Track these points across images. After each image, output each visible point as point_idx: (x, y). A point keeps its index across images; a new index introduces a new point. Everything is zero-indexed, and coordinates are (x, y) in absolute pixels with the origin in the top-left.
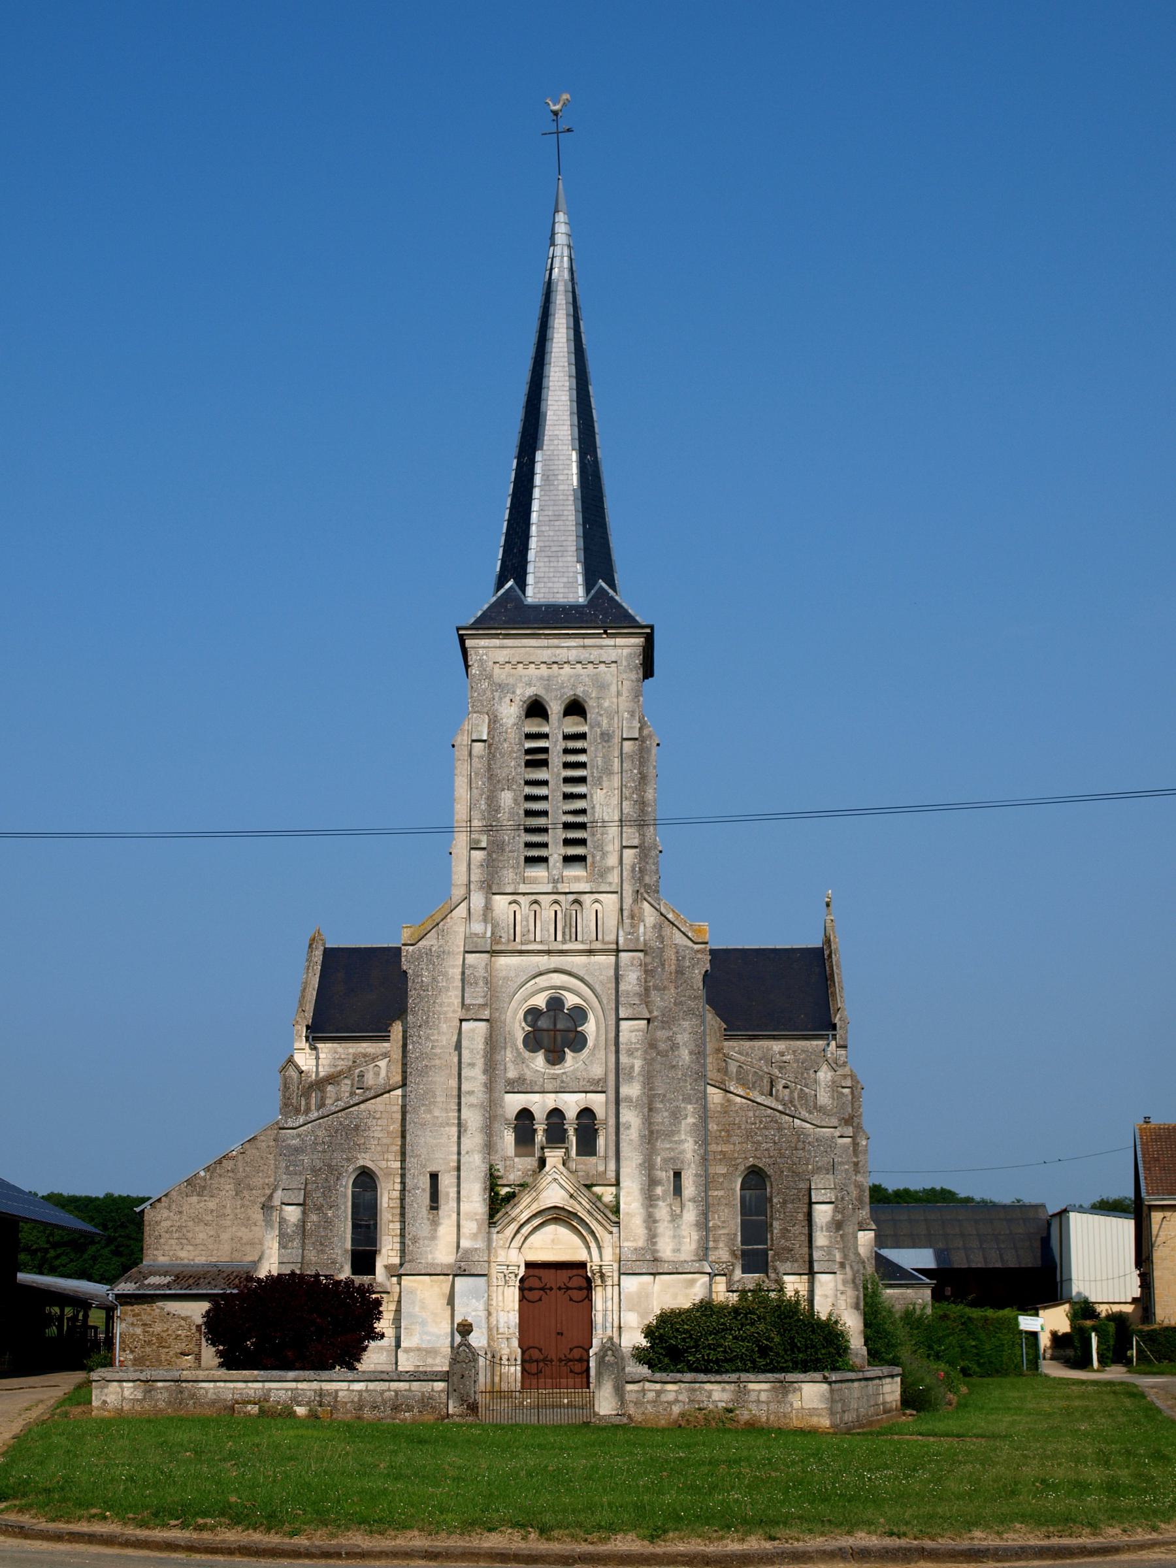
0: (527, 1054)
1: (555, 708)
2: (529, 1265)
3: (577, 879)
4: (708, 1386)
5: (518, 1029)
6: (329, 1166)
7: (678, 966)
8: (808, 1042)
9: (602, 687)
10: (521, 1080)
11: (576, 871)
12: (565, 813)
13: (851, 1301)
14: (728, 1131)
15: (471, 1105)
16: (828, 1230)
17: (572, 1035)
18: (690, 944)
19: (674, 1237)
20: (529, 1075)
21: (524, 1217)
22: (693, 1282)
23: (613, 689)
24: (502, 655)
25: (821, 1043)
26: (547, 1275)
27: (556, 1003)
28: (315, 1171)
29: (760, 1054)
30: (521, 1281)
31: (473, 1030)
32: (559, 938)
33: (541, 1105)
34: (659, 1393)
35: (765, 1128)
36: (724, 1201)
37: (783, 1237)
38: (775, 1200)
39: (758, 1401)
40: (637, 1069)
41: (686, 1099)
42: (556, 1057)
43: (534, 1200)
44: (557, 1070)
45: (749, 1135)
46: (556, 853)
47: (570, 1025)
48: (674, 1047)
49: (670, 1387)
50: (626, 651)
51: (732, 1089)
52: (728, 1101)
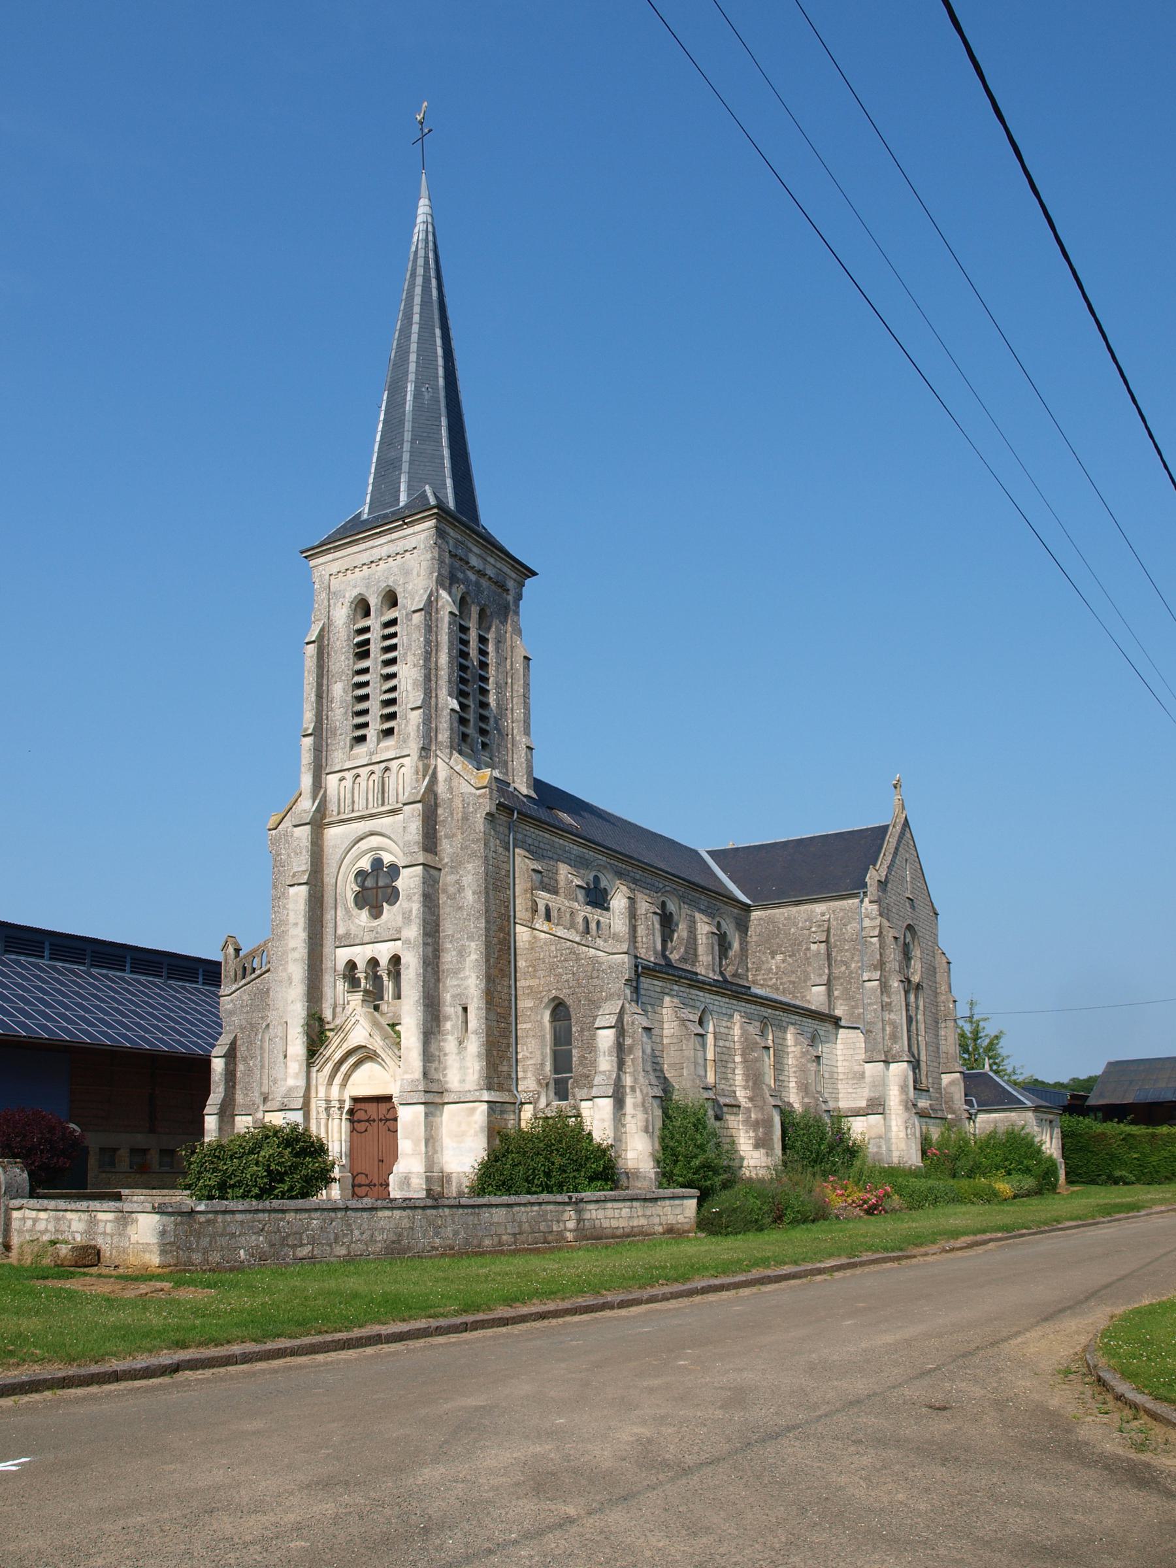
0: (355, 911)
1: (373, 602)
2: (355, 1100)
3: (387, 749)
4: (69, 1215)
5: (349, 889)
6: (251, 1024)
7: (464, 813)
8: (845, 902)
9: (407, 572)
10: (348, 935)
11: (390, 742)
12: (385, 692)
13: (641, 1124)
14: (534, 966)
15: (296, 960)
16: (610, 1055)
17: (389, 890)
18: (474, 791)
19: (460, 1068)
21: (337, 1056)
22: (473, 1110)
23: (415, 573)
24: (334, 568)
25: (856, 901)
26: (371, 1107)
27: (377, 863)
28: (242, 1029)
29: (805, 916)
30: (351, 1112)
31: (297, 894)
32: (370, 805)
33: (360, 955)
34: (35, 1220)
35: (566, 960)
36: (531, 1033)
37: (581, 1064)
38: (574, 1029)
39: (104, 1233)
40: (414, 912)
41: (471, 938)
42: (376, 913)
43: (343, 1040)
44: (376, 923)
45: (552, 968)
46: (371, 733)
47: (388, 881)
48: (461, 889)
49: (43, 1215)
50: (423, 535)
51: (537, 926)
52: (535, 937)
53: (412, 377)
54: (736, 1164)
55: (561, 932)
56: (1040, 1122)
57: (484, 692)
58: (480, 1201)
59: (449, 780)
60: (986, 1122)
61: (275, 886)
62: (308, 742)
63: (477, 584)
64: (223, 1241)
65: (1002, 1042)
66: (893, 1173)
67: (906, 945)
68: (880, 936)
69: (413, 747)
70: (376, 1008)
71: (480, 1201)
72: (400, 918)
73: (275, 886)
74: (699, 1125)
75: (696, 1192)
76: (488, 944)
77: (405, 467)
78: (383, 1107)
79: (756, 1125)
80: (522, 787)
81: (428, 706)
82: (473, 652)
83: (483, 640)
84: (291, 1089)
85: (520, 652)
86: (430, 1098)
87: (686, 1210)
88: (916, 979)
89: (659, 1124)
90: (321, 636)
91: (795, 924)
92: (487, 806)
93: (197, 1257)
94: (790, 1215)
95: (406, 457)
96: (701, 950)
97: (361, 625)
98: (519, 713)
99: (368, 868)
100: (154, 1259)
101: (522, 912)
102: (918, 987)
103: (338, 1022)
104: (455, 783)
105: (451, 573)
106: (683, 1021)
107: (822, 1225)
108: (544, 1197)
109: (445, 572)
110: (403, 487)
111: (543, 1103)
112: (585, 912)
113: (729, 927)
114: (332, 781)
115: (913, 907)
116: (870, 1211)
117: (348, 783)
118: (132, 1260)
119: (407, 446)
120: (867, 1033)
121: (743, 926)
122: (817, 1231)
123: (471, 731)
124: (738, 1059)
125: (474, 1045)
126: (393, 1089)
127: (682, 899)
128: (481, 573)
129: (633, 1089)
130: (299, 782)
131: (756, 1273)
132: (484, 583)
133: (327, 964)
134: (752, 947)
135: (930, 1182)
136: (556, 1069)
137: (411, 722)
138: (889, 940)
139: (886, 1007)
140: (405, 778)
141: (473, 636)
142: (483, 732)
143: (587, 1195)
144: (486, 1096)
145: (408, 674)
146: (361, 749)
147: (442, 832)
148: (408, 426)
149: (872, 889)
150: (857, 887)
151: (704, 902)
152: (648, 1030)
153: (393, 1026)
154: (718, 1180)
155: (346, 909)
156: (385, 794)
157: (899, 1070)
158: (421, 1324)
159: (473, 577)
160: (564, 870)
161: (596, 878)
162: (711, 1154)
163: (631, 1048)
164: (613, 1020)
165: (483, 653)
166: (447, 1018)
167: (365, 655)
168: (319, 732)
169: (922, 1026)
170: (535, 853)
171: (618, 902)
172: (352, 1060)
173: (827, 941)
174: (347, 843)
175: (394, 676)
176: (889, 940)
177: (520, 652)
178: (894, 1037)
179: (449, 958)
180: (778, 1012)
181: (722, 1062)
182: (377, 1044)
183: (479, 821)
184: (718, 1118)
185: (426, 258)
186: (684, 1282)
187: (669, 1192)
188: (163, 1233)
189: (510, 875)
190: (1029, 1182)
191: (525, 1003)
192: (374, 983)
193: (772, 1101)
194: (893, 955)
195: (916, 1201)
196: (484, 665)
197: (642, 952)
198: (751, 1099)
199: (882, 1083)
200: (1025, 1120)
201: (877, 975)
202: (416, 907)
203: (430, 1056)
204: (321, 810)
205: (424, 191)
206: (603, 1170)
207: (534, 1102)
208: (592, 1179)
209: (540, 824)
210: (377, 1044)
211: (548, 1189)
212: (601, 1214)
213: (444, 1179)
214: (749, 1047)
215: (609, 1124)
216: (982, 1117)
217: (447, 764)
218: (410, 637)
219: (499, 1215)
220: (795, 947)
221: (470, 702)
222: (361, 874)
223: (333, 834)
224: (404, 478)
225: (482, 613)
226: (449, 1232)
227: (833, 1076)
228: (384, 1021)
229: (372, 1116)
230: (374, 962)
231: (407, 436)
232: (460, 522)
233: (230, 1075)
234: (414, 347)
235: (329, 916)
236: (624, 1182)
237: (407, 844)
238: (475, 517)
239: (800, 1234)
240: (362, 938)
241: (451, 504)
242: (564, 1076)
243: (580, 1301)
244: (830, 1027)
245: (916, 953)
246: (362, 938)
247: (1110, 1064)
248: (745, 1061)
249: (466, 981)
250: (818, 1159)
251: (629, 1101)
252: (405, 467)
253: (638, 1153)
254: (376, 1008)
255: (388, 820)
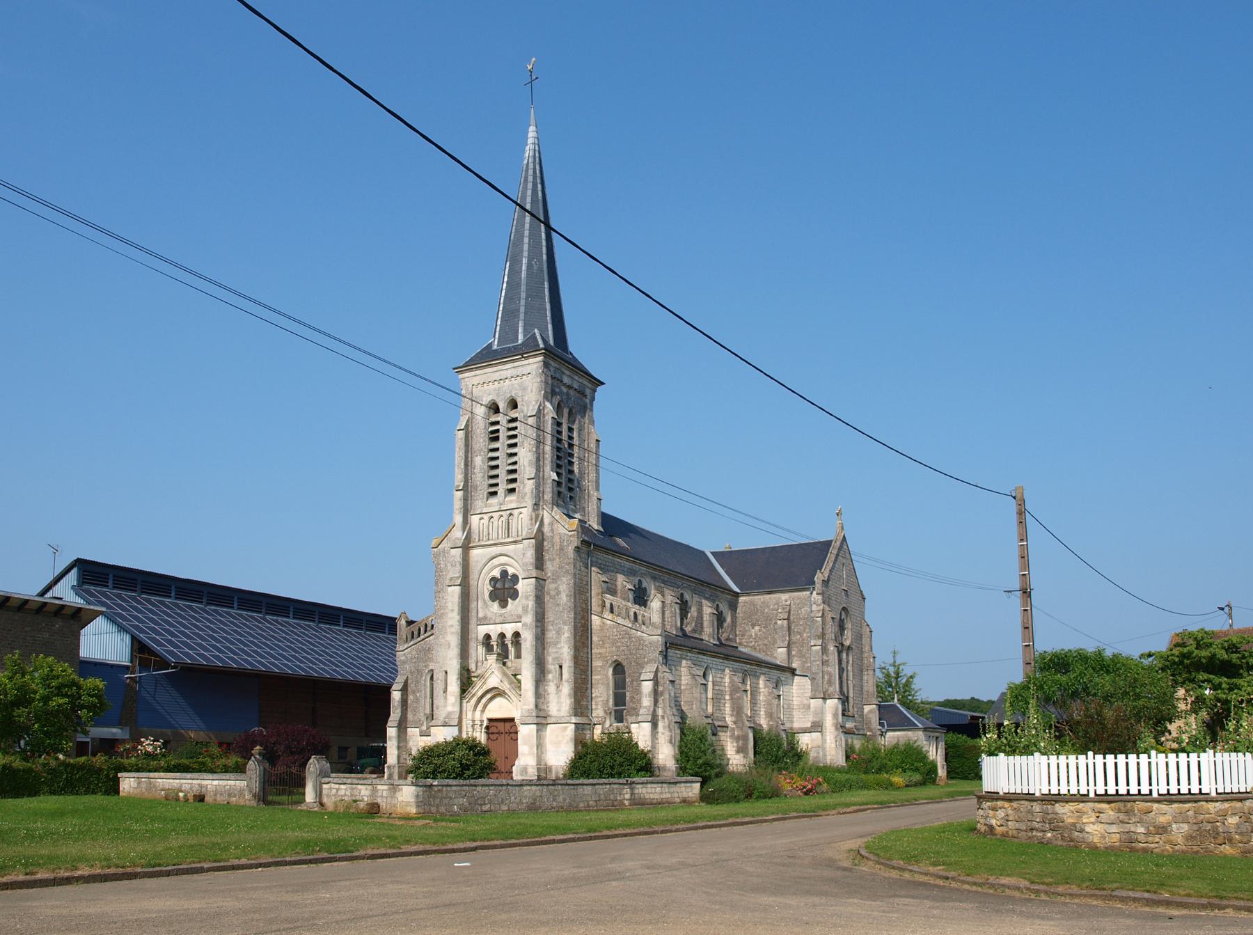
0: (490, 603)
1: (502, 406)
2: (490, 720)
3: (511, 502)
5: (486, 589)
9: (524, 389)
10: (485, 618)
11: (512, 497)
20: (489, 615)
21: (480, 694)
22: (565, 728)
24: (475, 381)
26: (500, 726)
28: (412, 673)
30: (487, 728)
33: (494, 630)
34: (338, 790)
41: (565, 623)
42: (504, 604)
43: (484, 683)
44: (503, 611)
46: (501, 490)
48: (559, 593)
53: (525, 254)
54: (725, 762)
55: (620, 620)
56: (928, 738)
57: (571, 463)
58: (569, 782)
59: (551, 524)
60: (893, 737)
61: (436, 584)
62: (460, 493)
63: (567, 394)
64: (446, 801)
65: (915, 680)
66: (825, 771)
67: (841, 621)
68: (823, 616)
69: (529, 502)
70: (504, 664)
71: (569, 782)
72: (520, 609)
73: (436, 584)
74: (703, 739)
75: (700, 779)
76: (575, 628)
77: (522, 316)
78: (508, 725)
79: (738, 739)
80: (595, 524)
81: (539, 478)
82: (565, 436)
83: (570, 430)
84: (450, 713)
85: (594, 437)
86: (540, 720)
87: (693, 789)
88: (847, 643)
89: (678, 738)
90: (467, 426)
91: (768, 607)
92: (576, 542)
93: (433, 809)
94: (756, 794)
95: (522, 309)
96: (706, 624)
97: (493, 419)
98: (593, 476)
99: (498, 576)
100: (413, 810)
101: (595, 603)
102: (849, 648)
103: (479, 672)
104: (555, 526)
105: (553, 389)
106: (694, 676)
107: (776, 800)
108: (612, 780)
109: (549, 390)
110: (520, 330)
111: (607, 724)
112: (635, 608)
113: (724, 608)
114: (474, 520)
115: (847, 595)
116: (806, 793)
117: (485, 521)
118: (399, 810)
119: (523, 302)
120: (812, 679)
121: (733, 607)
122: (772, 804)
123: (563, 489)
124: (727, 697)
125: (566, 689)
126: (516, 715)
127: (694, 591)
128: (570, 387)
129: (663, 717)
130: (452, 518)
131: (730, 820)
132: (572, 392)
133: (472, 635)
134: (739, 621)
135: (848, 776)
136: (616, 704)
137: (527, 487)
138: (829, 619)
139: (824, 663)
140: (523, 520)
141: (565, 428)
142: (570, 489)
143: (636, 779)
144: (574, 720)
145: (525, 455)
146: (493, 500)
147: (546, 557)
148: (523, 288)
149: (818, 586)
150: (809, 584)
151: (708, 592)
152: (672, 682)
153: (515, 675)
154: (713, 772)
155: (485, 602)
156: (511, 529)
157: (833, 704)
158: (571, 836)
159: (565, 390)
160: (620, 578)
161: (640, 582)
162: (709, 757)
163: (662, 693)
164: (651, 676)
165: (571, 438)
166: (550, 672)
167: (496, 439)
168: (467, 489)
169: (851, 674)
170: (604, 569)
171: (655, 604)
172: (488, 696)
173: (788, 619)
174: (484, 561)
175: (515, 454)
176: (829, 619)
177: (594, 437)
178: (830, 683)
179: (551, 635)
180: (753, 665)
181: (718, 699)
182: (505, 686)
183: (570, 551)
184: (714, 734)
185: (534, 169)
186: (693, 824)
187: (684, 779)
188: (417, 796)
189: (589, 583)
190: (917, 777)
191: (597, 663)
192: (504, 648)
193: (748, 724)
194: (831, 629)
195: (838, 787)
196: (571, 446)
197: (668, 628)
198: (735, 723)
199: (822, 712)
200: (917, 737)
201: (820, 642)
202: (531, 603)
203: (539, 695)
204: (468, 538)
205: (533, 121)
206: (644, 765)
207: (603, 724)
208: (639, 771)
209: (606, 550)
210: (505, 686)
211: (612, 776)
212: (644, 791)
213: (548, 769)
214: (734, 690)
215: (648, 738)
216: (889, 734)
217: (552, 516)
218: (526, 432)
219: (588, 790)
220: (768, 621)
221: (563, 471)
222: (493, 580)
223: (475, 553)
224: (521, 324)
225: (570, 413)
226: (561, 799)
227: (790, 708)
228: (509, 673)
229: (503, 728)
230: (502, 636)
231: (523, 295)
232: (558, 356)
233: (404, 702)
234: (527, 233)
235: (473, 605)
236: (657, 772)
237: (525, 564)
238: (565, 348)
239: (761, 805)
240: (497, 621)
241: (551, 342)
242: (621, 706)
243: (642, 829)
244: (789, 675)
245: (848, 625)
246: (497, 621)
247: (973, 698)
248: (732, 699)
249: (562, 649)
250: (777, 760)
251: (660, 724)
252: (522, 316)
253: (665, 755)
254: (504, 664)
255: (512, 547)
